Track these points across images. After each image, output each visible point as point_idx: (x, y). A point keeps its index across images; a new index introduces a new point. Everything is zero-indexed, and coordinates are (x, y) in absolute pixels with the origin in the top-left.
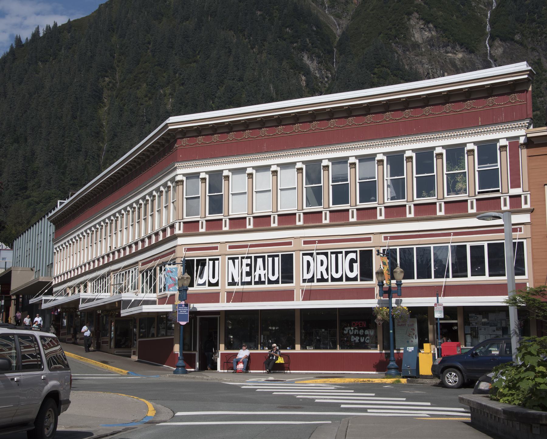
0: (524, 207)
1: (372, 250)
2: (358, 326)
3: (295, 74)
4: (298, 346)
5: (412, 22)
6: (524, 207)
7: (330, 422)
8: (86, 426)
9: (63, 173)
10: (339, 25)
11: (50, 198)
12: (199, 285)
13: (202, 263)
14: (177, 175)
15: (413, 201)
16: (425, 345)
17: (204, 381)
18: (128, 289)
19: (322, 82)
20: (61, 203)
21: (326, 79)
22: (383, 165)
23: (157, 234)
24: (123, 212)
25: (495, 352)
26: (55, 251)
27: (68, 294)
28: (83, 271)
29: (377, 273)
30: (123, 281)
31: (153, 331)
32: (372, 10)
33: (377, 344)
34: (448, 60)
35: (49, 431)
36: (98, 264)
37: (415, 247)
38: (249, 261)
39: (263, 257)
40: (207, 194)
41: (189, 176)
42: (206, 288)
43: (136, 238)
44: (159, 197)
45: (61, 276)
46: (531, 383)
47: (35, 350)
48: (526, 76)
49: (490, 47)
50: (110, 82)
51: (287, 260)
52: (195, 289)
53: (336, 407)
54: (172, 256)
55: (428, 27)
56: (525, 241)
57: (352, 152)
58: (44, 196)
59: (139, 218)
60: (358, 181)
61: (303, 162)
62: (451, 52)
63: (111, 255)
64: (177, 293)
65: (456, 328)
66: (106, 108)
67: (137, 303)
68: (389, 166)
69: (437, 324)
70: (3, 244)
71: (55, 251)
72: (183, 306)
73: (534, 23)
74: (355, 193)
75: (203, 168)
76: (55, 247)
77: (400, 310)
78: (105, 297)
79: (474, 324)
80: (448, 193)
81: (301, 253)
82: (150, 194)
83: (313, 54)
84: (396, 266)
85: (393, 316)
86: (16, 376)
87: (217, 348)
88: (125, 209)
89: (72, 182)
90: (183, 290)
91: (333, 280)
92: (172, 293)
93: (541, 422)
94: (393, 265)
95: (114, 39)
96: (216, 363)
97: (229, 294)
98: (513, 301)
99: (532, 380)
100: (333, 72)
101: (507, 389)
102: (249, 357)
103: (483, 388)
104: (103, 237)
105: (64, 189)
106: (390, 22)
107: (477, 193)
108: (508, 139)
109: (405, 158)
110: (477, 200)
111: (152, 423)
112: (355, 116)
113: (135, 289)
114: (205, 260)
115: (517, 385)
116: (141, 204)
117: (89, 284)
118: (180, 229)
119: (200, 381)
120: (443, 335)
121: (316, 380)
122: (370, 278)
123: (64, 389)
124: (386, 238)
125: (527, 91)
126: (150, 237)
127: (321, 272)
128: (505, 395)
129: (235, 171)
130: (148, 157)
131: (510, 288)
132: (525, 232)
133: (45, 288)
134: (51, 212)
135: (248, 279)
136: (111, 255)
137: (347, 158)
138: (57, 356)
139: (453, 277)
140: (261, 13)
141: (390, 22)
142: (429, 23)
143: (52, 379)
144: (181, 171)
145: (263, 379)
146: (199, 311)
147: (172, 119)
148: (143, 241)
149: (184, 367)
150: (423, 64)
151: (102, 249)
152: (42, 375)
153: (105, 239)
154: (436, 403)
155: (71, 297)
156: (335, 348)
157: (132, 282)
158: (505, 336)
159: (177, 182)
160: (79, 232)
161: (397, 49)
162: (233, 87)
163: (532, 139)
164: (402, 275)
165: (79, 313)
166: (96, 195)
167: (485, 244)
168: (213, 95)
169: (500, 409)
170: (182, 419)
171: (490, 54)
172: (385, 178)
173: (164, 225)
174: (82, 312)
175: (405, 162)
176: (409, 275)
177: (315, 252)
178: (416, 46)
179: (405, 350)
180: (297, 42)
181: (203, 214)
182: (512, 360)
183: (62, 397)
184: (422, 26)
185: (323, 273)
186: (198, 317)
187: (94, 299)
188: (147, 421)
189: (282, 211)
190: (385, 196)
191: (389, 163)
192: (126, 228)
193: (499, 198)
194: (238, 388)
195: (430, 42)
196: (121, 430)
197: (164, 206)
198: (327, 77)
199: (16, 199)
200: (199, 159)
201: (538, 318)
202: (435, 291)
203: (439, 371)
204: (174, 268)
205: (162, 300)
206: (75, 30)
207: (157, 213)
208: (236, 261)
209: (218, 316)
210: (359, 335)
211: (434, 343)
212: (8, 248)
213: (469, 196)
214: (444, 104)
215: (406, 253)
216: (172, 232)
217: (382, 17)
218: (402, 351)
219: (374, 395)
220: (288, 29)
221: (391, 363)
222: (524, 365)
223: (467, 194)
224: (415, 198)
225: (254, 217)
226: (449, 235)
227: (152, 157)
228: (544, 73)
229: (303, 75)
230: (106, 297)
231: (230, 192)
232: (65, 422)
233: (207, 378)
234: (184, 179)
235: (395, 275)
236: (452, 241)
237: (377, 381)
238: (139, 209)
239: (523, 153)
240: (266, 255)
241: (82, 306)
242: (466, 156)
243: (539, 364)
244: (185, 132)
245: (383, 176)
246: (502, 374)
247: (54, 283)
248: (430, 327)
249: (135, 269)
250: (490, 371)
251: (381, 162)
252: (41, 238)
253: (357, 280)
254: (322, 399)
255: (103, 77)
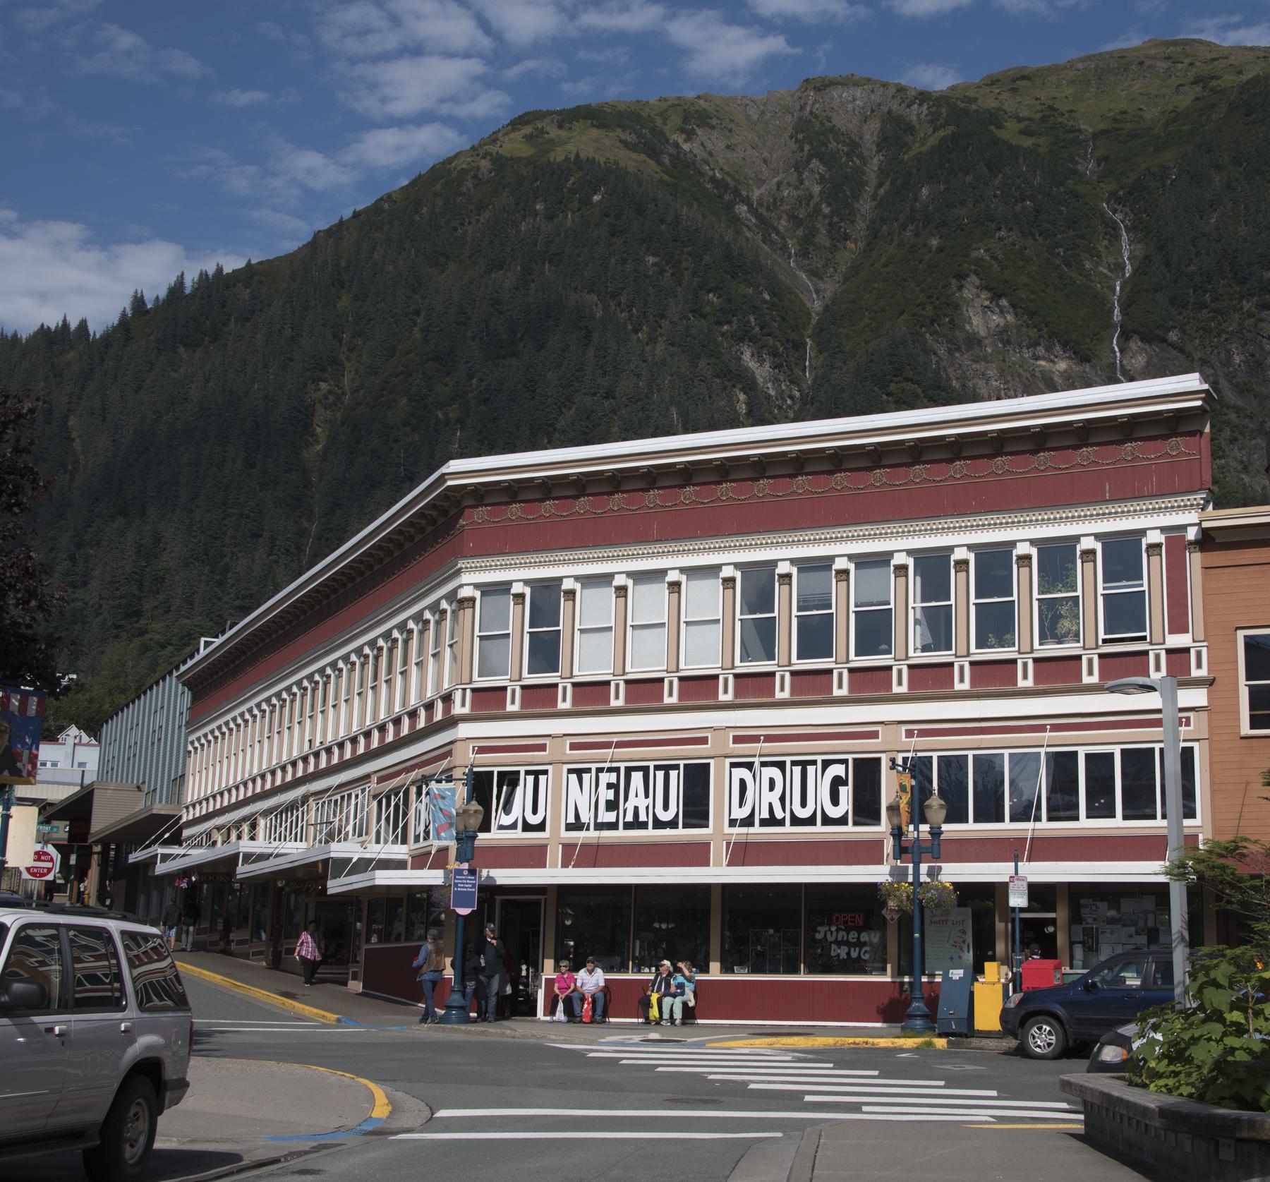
0: (1195, 673)
1: (879, 759)
2: (845, 922)
3: (725, 389)
4: (715, 966)
5: (967, 294)
6: (1195, 673)
7: (780, 1135)
8: (227, 1140)
9: (221, 583)
10: (817, 291)
11: (189, 635)
12: (501, 827)
13: (510, 780)
14: (461, 586)
15: (968, 655)
16: (987, 965)
17: (506, 1039)
18: (347, 834)
19: (780, 408)
20: (207, 644)
21: (789, 402)
22: (907, 576)
23: (413, 714)
24: (341, 664)
25: (1133, 980)
26: (190, 748)
27: (214, 843)
28: (250, 794)
29: (889, 808)
30: (335, 816)
31: (400, 927)
32: (885, 265)
33: (885, 963)
34: (1038, 374)
35: (135, 1150)
36: (283, 778)
37: (970, 754)
38: (612, 778)
39: (645, 770)
40: (527, 629)
41: (489, 590)
42: (518, 834)
43: (368, 723)
44: (421, 632)
45: (200, 803)
46: (1216, 1050)
47: (109, 967)
48: (1199, 403)
49: (1121, 351)
50: (330, 392)
51: (697, 778)
52: (493, 836)
53: (793, 1100)
54: (444, 764)
55: (998, 305)
56: (1196, 745)
57: (841, 547)
58: (176, 631)
59: (375, 678)
60: (852, 608)
61: (737, 566)
62: (1044, 358)
63: (312, 760)
64: (453, 845)
65: (1051, 929)
66: (319, 447)
67: (364, 865)
68: (918, 579)
69: (1013, 921)
70: (83, 734)
71: (190, 748)
72: (466, 873)
73: (1205, 311)
74: (845, 634)
75: (520, 573)
76: (193, 737)
77: (937, 890)
78: (294, 851)
79: (1090, 921)
80: (1040, 639)
81: (728, 761)
82: (402, 626)
83: (763, 347)
84: (931, 794)
85: (921, 901)
86: (60, 1023)
87: (537, 968)
88: (346, 658)
89: (238, 602)
90: (465, 839)
91: (796, 821)
92: (444, 843)
93: (1238, 1135)
94: (922, 792)
95: (344, 302)
96: (536, 1001)
97: (568, 848)
98: (1178, 870)
99: (1217, 1041)
100: (805, 386)
101: (1166, 1061)
102: (608, 987)
103: (1108, 1059)
104: (297, 719)
105: (220, 616)
106: (922, 291)
107: (1100, 643)
108: (1163, 529)
109: (952, 563)
110: (1101, 656)
111: (380, 1133)
112: (850, 470)
113: (360, 835)
114: (518, 772)
115: (1187, 1054)
116: (381, 649)
117: (262, 822)
118: (463, 705)
119: (498, 1039)
120: (1025, 944)
121: (752, 1041)
122: (876, 819)
123: (174, 1054)
124: (909, 734)
125: (1202, 433)
126: (397, 722)
127: (770, 804)
128: (1160, 1076)
129: (589, 581)
130: (400, 545)
131: (1173, 843)
132: (1197, 726)
133: (166, 828)
134: (184, 662)
135: (610, 817)
136: (312, 760)
137: (831, 559)
138: (165, 980)
139: (1050, 819)
140: (657, 260)
141: (922, 291)
142: (1000, 297)
143: (150, 1030)
144: (472, 577)
145: (637, 1038)
146: (501, 886)
147: (455, 465)
148: (382, 729)
149: (462, 1008)
150: (988, 380)
151: (292, 745)
152: (122, 1020)
153: (299, 723)
154: (1008, 1092)
155: (222, 850)
156: (796, 971)
157: (355, 818)
158: (1154, 948)
159: (462, 602)
160: (244, 708)
161: (936, 346)
162: (593, 411)
163: (1211, 533)
164: (943, 814)
165: (237, 886)
166: (282, 627)
167: (1117, 750)
168: (551, 425)
169: (1152, 1106)
170: (450, 1124)
171: (1122, 366)
172: (911, 604)
173: (429, 695)
174: (242, 881)
175: (953, 571)
176: (957, 815)
177: (757, 760)
178: (974, 341)
179: (946, 975)
180: (729, 323)
181: (516, 672)
182: (1173, 999)
183: (170, 1074)
184: (987, 303)
185: (774, 809)
186: (498, 898)
187: (271, 855)
188: (370, 1129)
189: (688, 669)
190: (910, 644)
191: (919, 572)
192: (346, 701)
193: (1146, 653)
194: (580, 1055)
195: (1002, 335)
196: (307, 1149)
197: (431, 652)
198: (792, 397)
199: (116, 637)
200: (510, 553)
201: (1229, 907)
202: (1010, 850)
203: (1016, 1021)
204: (449, 790)
205: (420, 861)
206: (260, 282)
207: (414, 668)
208: (586, 777)
209: (542, 897)
210: (847, 943)
211: (1007, 961)
212: (94, 742)
213: (1084, 648)
214: (1034, 452)
215: (953, 766)
216: (447, 710)
217: (906, 280)
218: (938, 979)
219: (876, 1073)
220: (711, 295)
221: (915, 1004)
222: (1201, 1008)
223: (1081, 644)
224: (973, 649)
225: (627, 682)
226: (1042, 729)
227: (408, 545)
228: (1225, 410)
229: (741, 390)
230: (295, 850)
231: (577, 626)
232: (174, 1131)
233: (513, 1033)
234: (478, 594)
235: (928, 813)
236: (1047, 743)
237: (883, 1042)
238: (377, 658)
239: (1195, 561)
240: (651, 764)
241: (243, 870)
242: (1079, 562)
243: (1233, 1007)
244: (482, 494)
245: (906, 601)
246: (1155, 1028)
247: (184, 819)
248: (1000, 926)
249: (363, 790)
250: (1126, 1022)
251: (901, 570)
252: (160, 719)
253: (846, 824)
254: (763, 1082)
255: (316, 380)
